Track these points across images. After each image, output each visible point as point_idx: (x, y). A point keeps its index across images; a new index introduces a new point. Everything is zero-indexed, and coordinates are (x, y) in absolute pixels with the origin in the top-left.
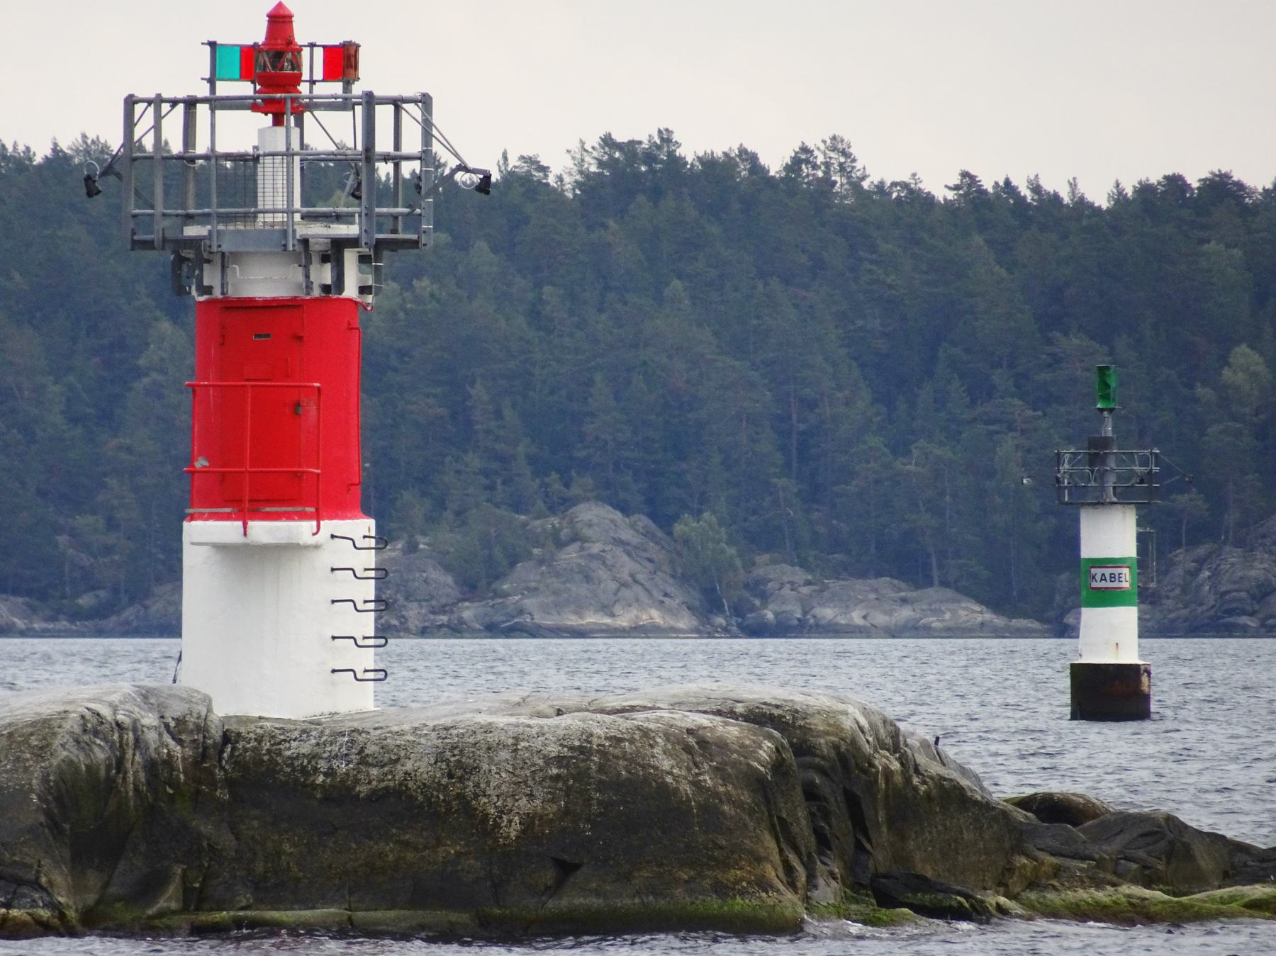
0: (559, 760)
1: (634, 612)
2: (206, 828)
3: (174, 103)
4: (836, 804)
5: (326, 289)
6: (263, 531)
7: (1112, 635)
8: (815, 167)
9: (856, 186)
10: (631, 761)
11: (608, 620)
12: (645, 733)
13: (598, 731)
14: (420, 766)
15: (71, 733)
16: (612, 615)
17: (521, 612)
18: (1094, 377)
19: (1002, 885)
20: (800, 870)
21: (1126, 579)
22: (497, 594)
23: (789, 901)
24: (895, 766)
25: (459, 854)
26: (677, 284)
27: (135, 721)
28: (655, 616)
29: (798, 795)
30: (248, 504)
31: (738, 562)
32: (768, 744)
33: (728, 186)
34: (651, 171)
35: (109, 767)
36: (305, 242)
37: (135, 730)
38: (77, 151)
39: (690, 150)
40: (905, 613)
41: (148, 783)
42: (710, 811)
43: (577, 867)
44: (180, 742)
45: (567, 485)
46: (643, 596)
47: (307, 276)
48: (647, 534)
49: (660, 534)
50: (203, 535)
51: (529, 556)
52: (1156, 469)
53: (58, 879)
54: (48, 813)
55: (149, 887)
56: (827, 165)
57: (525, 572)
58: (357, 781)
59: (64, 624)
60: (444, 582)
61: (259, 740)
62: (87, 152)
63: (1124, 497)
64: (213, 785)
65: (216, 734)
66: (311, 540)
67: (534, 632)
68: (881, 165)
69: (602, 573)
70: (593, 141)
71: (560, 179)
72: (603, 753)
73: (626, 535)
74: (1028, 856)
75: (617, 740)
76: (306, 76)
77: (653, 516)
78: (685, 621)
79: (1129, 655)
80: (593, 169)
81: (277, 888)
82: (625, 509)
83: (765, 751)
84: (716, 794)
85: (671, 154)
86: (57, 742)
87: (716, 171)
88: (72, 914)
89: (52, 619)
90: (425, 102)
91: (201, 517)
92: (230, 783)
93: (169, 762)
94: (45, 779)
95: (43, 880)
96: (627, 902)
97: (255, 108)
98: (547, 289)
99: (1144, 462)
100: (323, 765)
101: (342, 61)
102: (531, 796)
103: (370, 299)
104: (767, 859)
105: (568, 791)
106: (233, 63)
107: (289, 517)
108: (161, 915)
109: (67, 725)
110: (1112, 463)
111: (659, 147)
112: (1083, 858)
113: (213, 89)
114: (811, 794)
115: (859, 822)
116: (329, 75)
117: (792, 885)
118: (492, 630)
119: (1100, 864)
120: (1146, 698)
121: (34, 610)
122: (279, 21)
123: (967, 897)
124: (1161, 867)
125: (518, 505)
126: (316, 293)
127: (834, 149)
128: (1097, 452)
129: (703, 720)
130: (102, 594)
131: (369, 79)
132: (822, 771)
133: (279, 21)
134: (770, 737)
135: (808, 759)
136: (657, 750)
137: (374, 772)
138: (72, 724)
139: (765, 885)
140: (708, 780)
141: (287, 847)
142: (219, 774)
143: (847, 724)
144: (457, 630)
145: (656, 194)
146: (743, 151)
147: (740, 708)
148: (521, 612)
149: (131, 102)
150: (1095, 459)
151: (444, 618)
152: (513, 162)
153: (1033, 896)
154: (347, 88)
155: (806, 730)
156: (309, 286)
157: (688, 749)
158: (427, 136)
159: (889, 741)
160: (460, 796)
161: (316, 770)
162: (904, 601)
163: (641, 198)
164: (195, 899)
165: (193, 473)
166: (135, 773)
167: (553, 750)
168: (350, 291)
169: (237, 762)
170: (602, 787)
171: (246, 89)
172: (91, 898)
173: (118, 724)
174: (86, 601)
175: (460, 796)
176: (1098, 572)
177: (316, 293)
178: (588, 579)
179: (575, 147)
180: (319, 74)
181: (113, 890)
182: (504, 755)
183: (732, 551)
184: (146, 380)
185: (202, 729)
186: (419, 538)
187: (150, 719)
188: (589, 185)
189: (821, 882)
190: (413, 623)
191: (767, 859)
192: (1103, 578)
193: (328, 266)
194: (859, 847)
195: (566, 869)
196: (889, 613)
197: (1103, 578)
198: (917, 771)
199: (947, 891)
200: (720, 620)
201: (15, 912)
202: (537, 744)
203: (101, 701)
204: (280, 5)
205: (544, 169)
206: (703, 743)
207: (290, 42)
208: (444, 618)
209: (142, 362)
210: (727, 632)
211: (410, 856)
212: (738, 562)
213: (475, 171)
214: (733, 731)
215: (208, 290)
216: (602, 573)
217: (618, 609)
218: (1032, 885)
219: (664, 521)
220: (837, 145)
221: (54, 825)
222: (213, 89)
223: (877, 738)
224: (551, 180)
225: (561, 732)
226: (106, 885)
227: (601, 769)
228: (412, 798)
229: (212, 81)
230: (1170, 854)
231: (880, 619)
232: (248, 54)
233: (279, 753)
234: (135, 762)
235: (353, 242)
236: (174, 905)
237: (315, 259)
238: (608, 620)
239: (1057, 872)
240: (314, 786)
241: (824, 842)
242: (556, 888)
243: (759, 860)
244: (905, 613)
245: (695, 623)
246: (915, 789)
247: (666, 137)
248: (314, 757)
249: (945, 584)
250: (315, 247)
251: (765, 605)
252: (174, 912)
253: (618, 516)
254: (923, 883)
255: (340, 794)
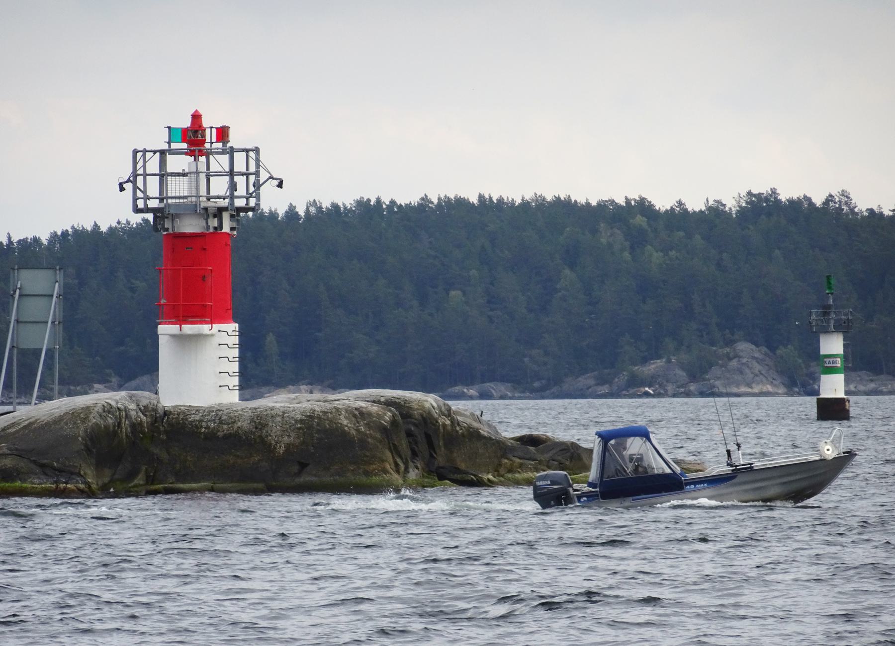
0: (301, 421)
1: (760, 386)
2: (156, 451)
3: (155, 152)
4: (421, 438)
5: (215, 228)
6: (188, 329)
7: (833, 386)
8: (835, 203)
9: (852, 210)
10: (331, 421)
11: (750, 390)
12: (337, 409)
13: (318, 409)
14: (244, 424)
15: (98, 412)
16: (751, 388)
17: (714, 387)
18: (825, 279)
19: (496, 471)
20: (402, 467)
21: (839, 363)
22: (704, 380)
23: (397, 478)
24: (448, 422)
25: (259, 460)
26: (777, 252)
27: (125, 407)
28: (770, 388)
29: (403, 435)
30: (182, 316)
31: (803, 366)
32: (389, 414)
33: (799, 211)
34: (768, 205)
35: (114, 426)
36: (206, 209)
37: (126, 411)
38: (533, 200)
39: (783, 197)
40: (872, 386)
41: (132, 433)
42: (363, 442)
43: (307, 465)
44: (145, 415)
45: (733, 335)
46: (764, 379)
47: (207, 223)
48: (766, 354)
49: (771, 354)
50: (166, 330)
51: (717, 364)
52: (851, 317)
53: (89, 472)
54: (86, 445)
55: (132, 475)
56: (840, 202)
57: (716, 371)
58: (218, 431)
59: (528, 394)
60: (681, 374)
61: (179, 414)
62: (537, 200)
63: (838, 329)
64: (159, 433)
65: (161, 412)
66: (208, 332)
67: (720, 395)
68: (863, 203)
69: (747, 371)
70: (744, 193)
71: (730, 209)
72: (319, 418)
73: (757, 355)
74: (508, 459)
75: (325, 413)
76: (208, 139)
77: (768, 347)
78: (781, 390)
79: (841, 394)
80: (744, 205)
81: (185, 475)
82: (757, 345)
83: (388, 416)
84: (366, 435)
85: (776, 198)
86: (91, 416)
87: (795, 205)
88: (94, 486)
89: (523, 392)
90: (257, 150)
91: (165, 323)
92: (166, 432)
93: (141, 424)
94: (86, 431)
95: (82, 473)
96: (328, 479)
97: (186, 154)
98: (725, 254)
99: (845, 314)
100: (204, 424)
101: (222, 134)
102: (289, 436)
103: (235, 233)
104: (386, 461)
105: (304, 434)
106: (179, 136)
107: (201, 323)
108: (135, 486)
109: (96, 409)
110: (833, 316)
111: (771, 196)
112: (533, 460)
113: (170, 146)
114: (409, 434)
115: (431, 445)
116: (218, 141)
117: (398, 472)
118: (702, 394)
119: (540, 462)
120: (848, 411)
121: (515, 389)
122: (196, 117)
123: (475, 476)
124: (568, 463)
125: (712, 344)
126: (211, 230)
127: (843, 195)
128: (826, 311)
129: (363, 404)
130: (544, 382)
131: (234, 141)
132: (415, 425)
133: (196, 117)
134: (390, 411)
135: (409, 420)
136: (342, 417)
137: (225, 427)
138: (99, 408)
139: (385, 471)
140: (362, 428)
141: (189, 458)
142: (162, 428)
143: (427, 405)
144: (688, 394)
145: (769, 215)
146: (805, 197)
147: (383, 399)
148: (714, 387)
149: (135, 152)
150: (825, 314)
151: (682, 390)
152: (711, 203)
153: (510, 475)
154: (225, 144)
155: (410, 408)
156: (208, 227)
157: (355, 416)
158: (258, 166)
159: (446, 412)
160: (260, 436)
161: (201, 426)
162: (872, 381)
163: (763, 217)
164: (150, 480)
165: (160, 305)
166: (126, 429)
167: (299, 417)
168: (226, 229)
169: (170, 424)
170: (318, 432)
171: (184, 146)
172: (106, 480)
173: (119, 409)
174: (536, 384)
175: (260, 436)
176: (827, 360)
177: (211, 230)
178: (741, 373)
179: (736, 196)
180: (214, 140)
181: (117, 476)
182: (279, 419)
183: (800, 361)
184: (560, 294)
185: (155, 410)
186: (672, 357)
187: (132, 406)
188: (742, 211)
189: (411, 470)
190: (670, 392)
191: (386, 461)
192: (829, 363)
193: (216, 219)
194: (431, 456)
195: (303, 466)
196: (865, 385)
197: (829, 363)
198: (459, 425)
199: (467, 473)
200: (796, 389)
201: (69, 486)
202: (292, 415)
203: (111, 399)
204: (196, 111)
205: (724, 205)
206: (361, 413)
207: (200, 126)
208: (682, 390)
209: (558, 286)
210: (799, 394)
211: (239, 461)
212: (803, 366)
213: (276, 179)
214: (375, 408)
215: (167, 230)
216: (747, 371)
217: (754, 385)
218: (510, 471)
219: (772, 348)
220: (844, 193)
221: (88, 450)
222: (170, 146)
223: (441, 411)
224: (727, 209)
225: (302, 410)
226: (114, 474)
227: (318, 425)
228: (241, 437)
229: (169, 143)
230: (571, 458)
231: (862, 388)
232: (185, 131)
233: (187, 420)
234: (125, 424)
235: (225, 209)
236: (141, 482)
237: (211, 216)
238: (750, 390)
239: (521, 466)
240: (201, 433)
241: (414, 454)
242: (299, 474)
243: (383, 461)
244: (872, 386)
245: (785, 390)
246: (457, 432)
247: (774, 191)
248: (201, 421)
249: (889, 373)
250: (210, 211)
251: (814, 383)
252: (141, 485)
253: (753, 347)
254: (458, 470)
255: (211, 436)
